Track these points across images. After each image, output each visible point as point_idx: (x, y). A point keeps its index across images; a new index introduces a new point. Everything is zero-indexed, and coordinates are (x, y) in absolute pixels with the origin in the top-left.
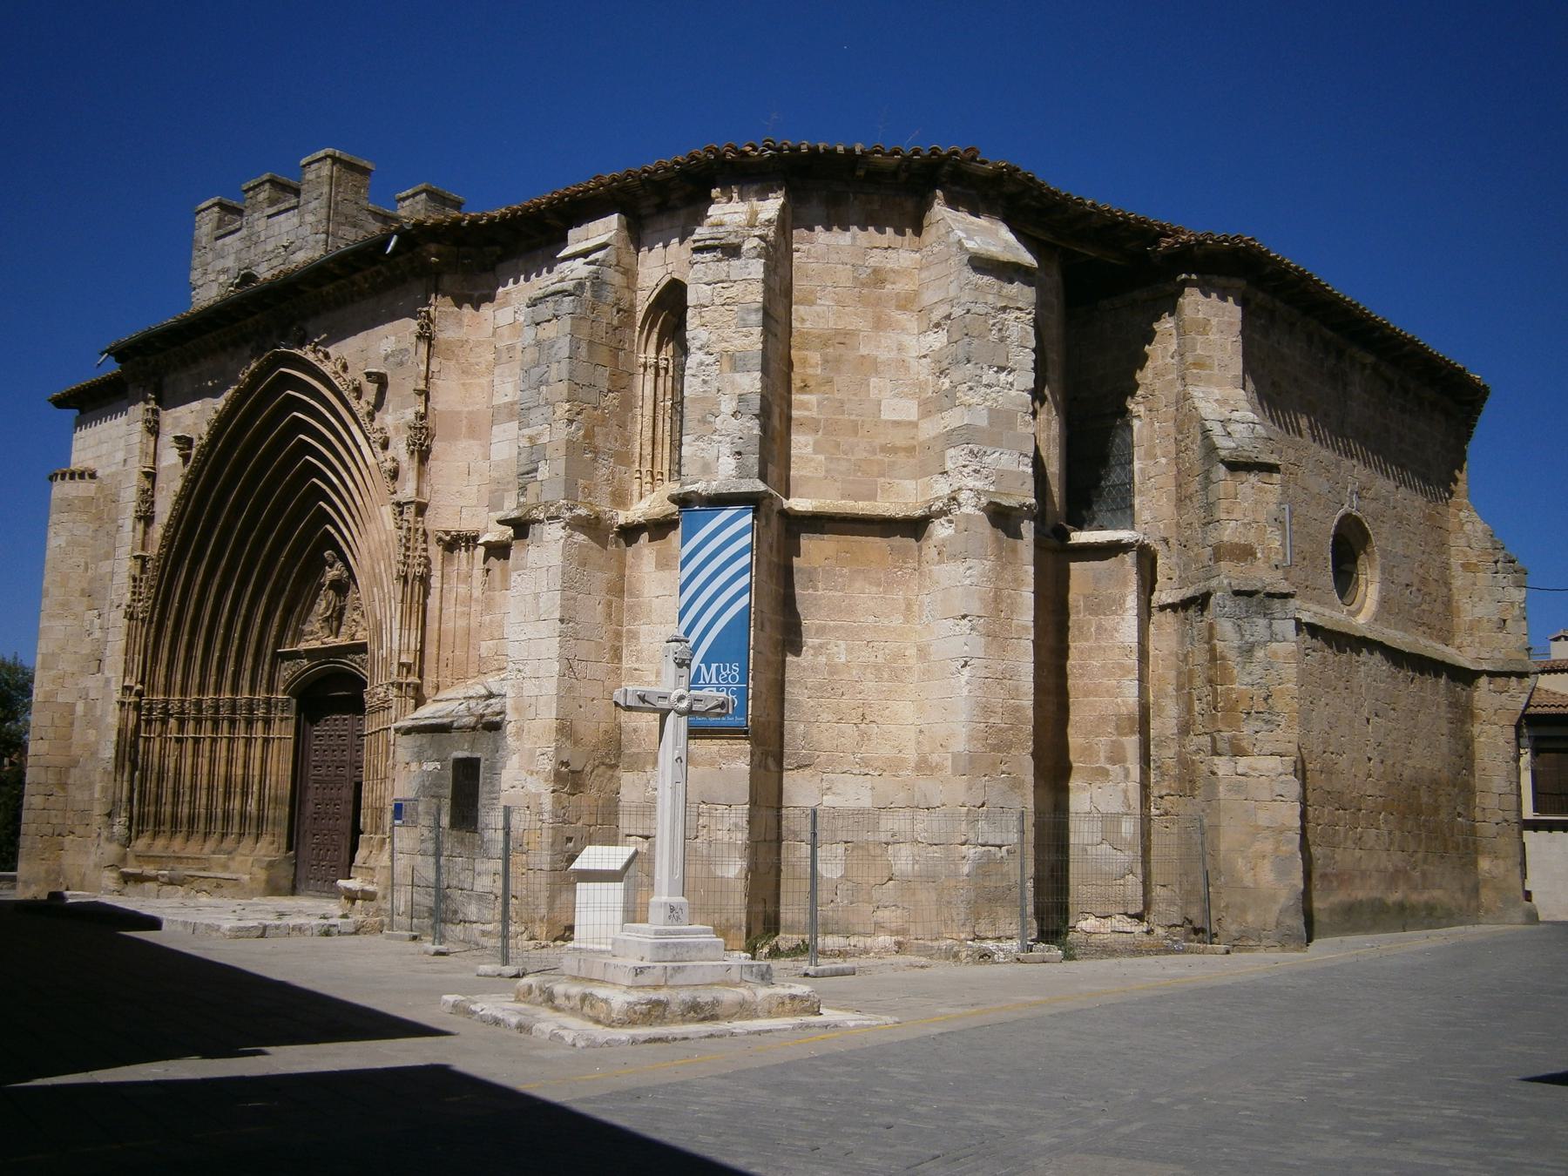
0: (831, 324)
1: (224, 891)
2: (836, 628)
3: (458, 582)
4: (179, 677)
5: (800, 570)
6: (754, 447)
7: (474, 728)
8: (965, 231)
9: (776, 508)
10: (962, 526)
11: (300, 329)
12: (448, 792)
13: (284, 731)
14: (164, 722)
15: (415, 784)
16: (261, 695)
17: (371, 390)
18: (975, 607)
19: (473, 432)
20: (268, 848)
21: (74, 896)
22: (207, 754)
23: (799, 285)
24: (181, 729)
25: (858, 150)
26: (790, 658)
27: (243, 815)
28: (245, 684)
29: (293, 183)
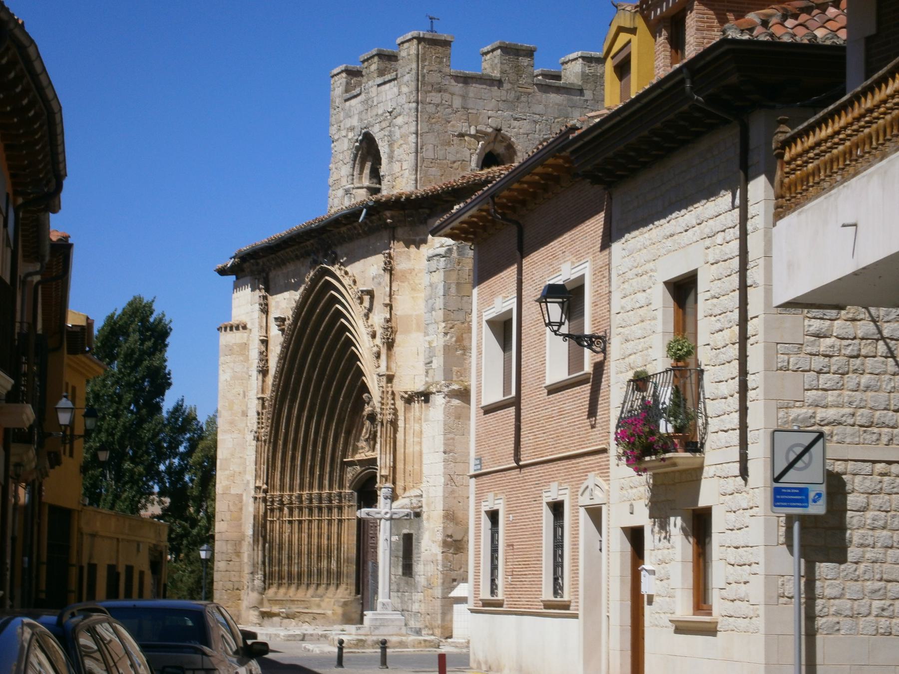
1: (318, 622)
14: (281, 510)
16: (336, 491)
17: (367, 298)
20: (344, 592)
22: (306, 531)
28: (326, 482)
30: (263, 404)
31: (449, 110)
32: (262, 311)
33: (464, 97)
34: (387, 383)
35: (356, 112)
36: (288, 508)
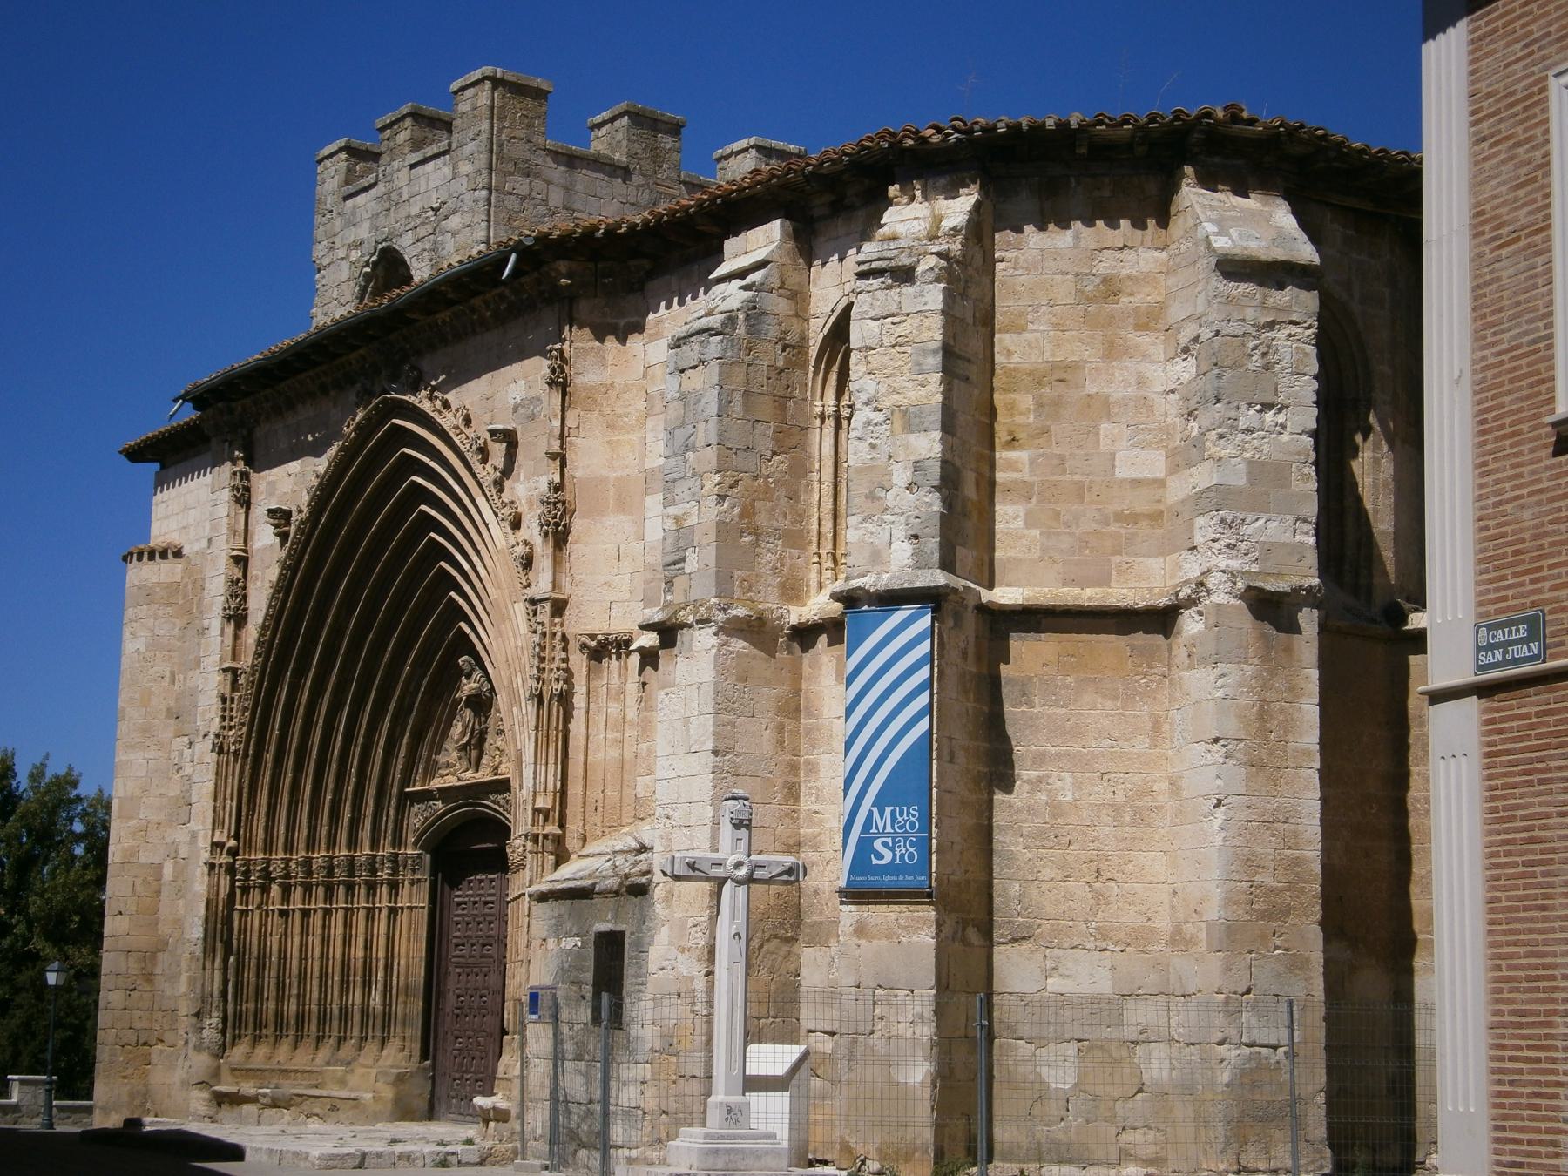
0: (1047, 356)
1: (341, 1115)
2: (1059, 756)
3: (607, 697)
4: (282, 828)
5: (1010, 681)
6: (934, 528)
7: (617, 893)
8: (1218, 222)
9: (971, 602)
10: (1212, 621)
11: (413, 368)
12: (589, 976)
13: (415, 897)
14: (265, 889)
15: (553, 967)
16: (386, 850)
17: (498, 450)
18: (1232, 728)
19: (622, 506)
20: (397, 1056)
21: (151, 1123)
22: (319, 931)
23: (1004, 307)
24: (286, 897)
25: (1074, 123)
26: (999, 797)
27: (365, 1012)
28: (365, 835)
29: (444, 113)
30: (234, 682)
31: (543, 210)
32: (238, 500)
33: (568, 189)
34: (553, 616)
35: (365, 216)
36: (281, 885)
